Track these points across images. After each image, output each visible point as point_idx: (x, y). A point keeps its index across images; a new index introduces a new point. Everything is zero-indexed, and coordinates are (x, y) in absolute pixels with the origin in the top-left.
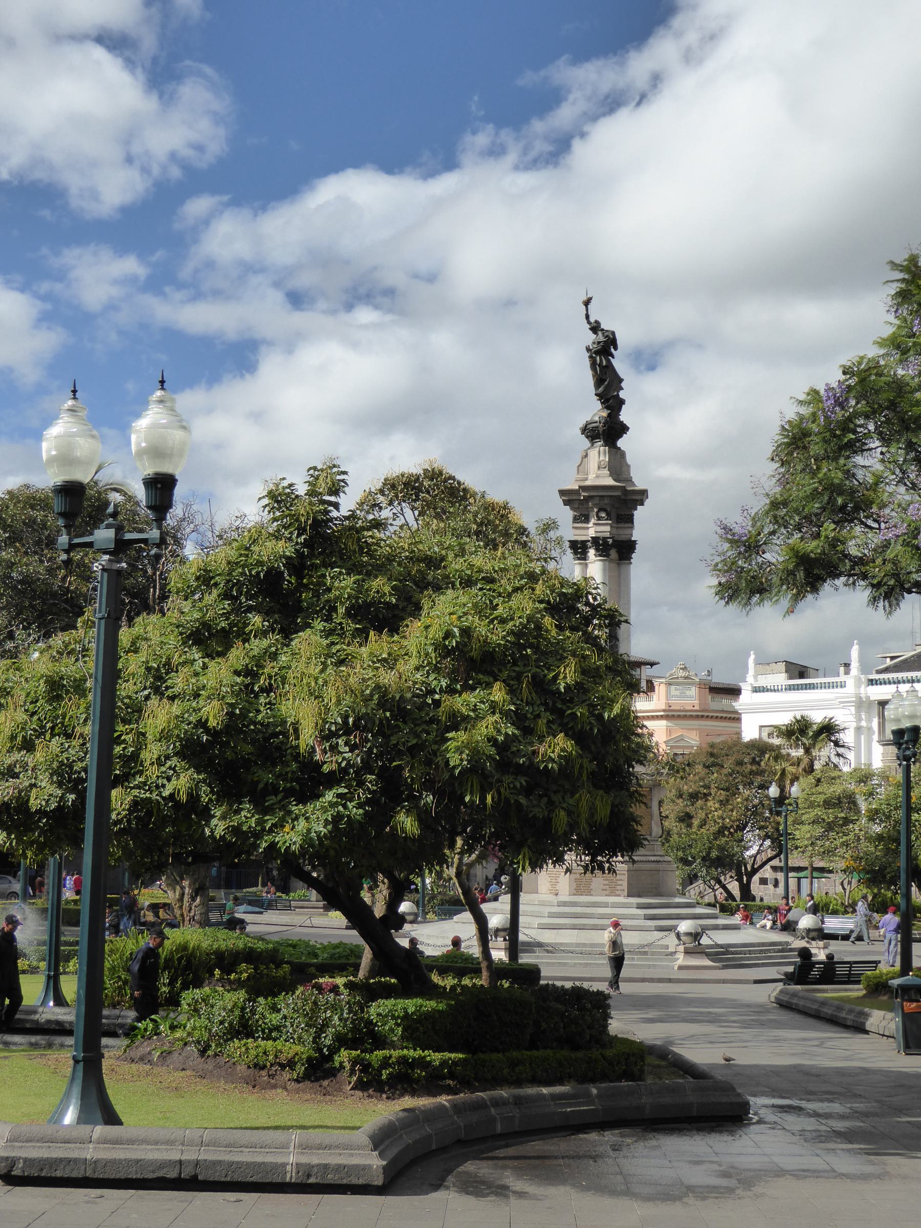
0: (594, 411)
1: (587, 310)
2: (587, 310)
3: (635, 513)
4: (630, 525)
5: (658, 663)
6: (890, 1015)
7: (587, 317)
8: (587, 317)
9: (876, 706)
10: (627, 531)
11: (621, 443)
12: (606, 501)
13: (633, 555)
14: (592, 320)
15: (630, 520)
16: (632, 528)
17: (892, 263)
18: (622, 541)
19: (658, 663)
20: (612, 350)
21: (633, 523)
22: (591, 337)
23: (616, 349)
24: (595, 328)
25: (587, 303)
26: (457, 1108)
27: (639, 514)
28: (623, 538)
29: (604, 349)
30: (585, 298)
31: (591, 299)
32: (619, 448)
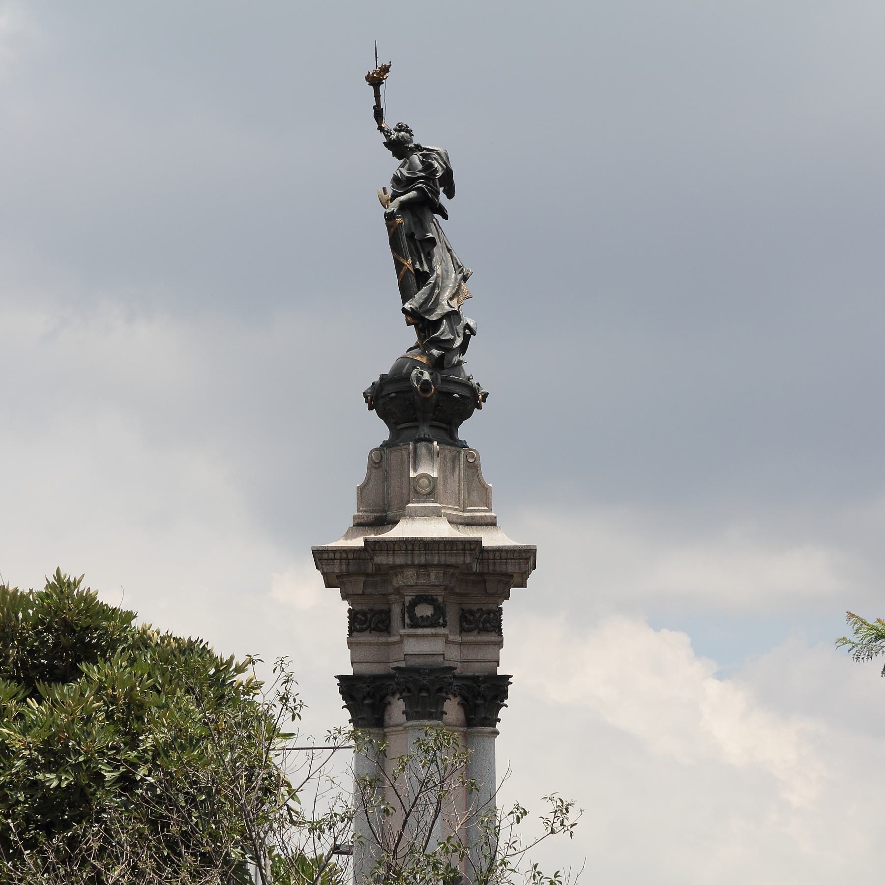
1: (377, 96)
2: (377, 96)
3: (505, 605)
4: (492, 637)
5: (58, 569)
6: (350, 801)
7: (378, 114)
8: (378, 114)
10: (484, 654)
13: (502, 713)
14: (390, 123)
15: (491, 624)
18: (475, 679)
19: (58, 569)
20: (443, 198)
21: (499, 631)
22: (392, 165)
23: (450, 194)
24: (399, 147)
25: (376, 81)
26: (356, 822)
27: (516, 611)
28: (476, 669)
30: (372, 69)
31: (385, 69)
32: (463, 445)
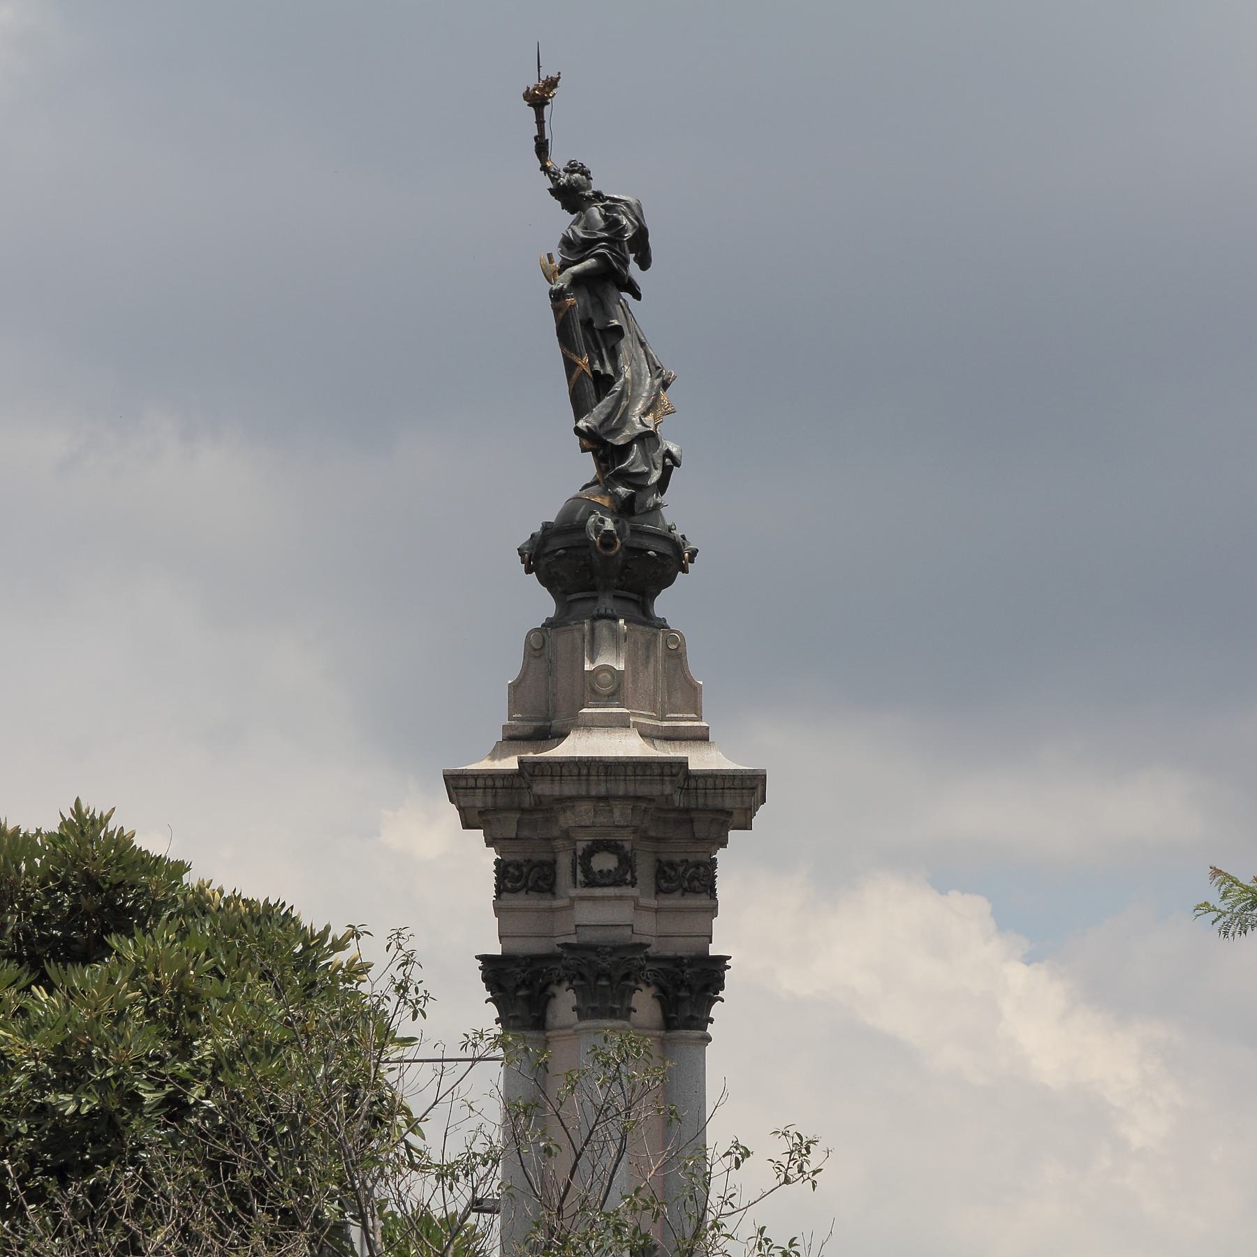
0: (559, 477)
1: (540, 122)
2: (540, 122)
7: (542, 148)
8: (542, 148)
9: (546, 857)
11: (664, 604)
12: (619, 814)
13: (716, 1010)
14: (558, 160)
16: (713, 911)
17: (722, 1001)
18: (677, 961)
20: (633, 269)
21: (711, 890)
22: (561, 221)
23: (644, 263)
24: (571, 195)
25: (537, 101)
28: (679, 947)
29: (600, 269)
30: (532, 82)
31: (552, 83)
32: (662, 625)
